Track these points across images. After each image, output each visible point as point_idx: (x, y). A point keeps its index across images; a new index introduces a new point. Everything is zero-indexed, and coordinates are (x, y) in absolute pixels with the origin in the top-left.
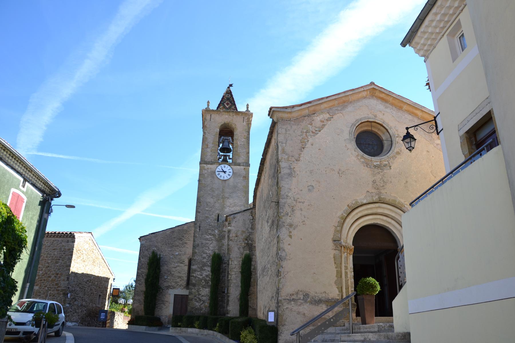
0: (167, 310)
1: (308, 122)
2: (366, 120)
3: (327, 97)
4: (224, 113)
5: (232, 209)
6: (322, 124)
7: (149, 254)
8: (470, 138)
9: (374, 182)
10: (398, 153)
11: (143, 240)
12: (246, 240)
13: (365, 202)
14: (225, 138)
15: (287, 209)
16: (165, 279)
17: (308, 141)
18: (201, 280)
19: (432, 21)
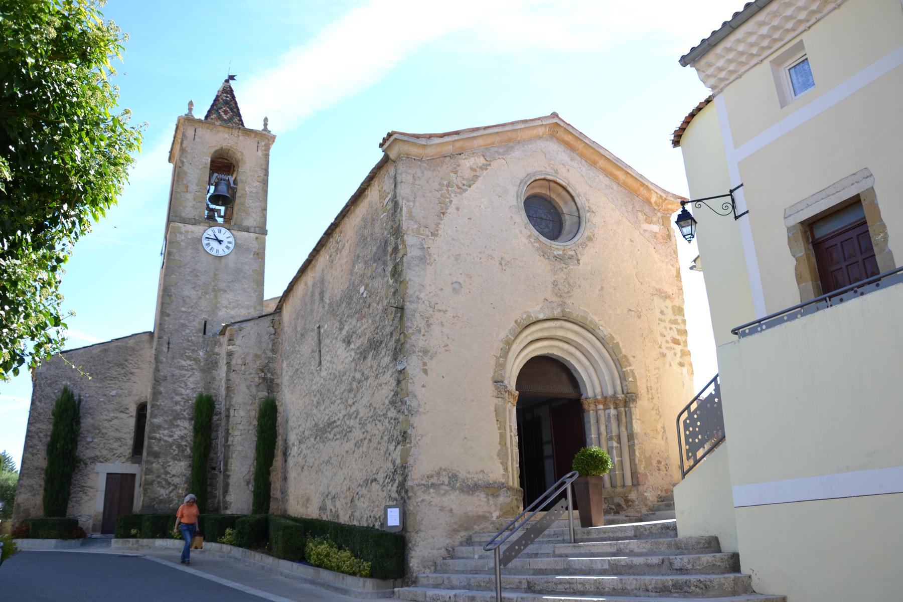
0: (91, 504)
1: (450, 168)
2: (542, 177)
3: (485, 128)
4: (222, 129)
5: (233, 313)
6: (473, 173)
7: (54, 394)
8: (806, 232)
9: (555, 284)
10: (590, 239)
12: (263, 371)
13: (541, 316)
14: (220, 176)
16: (88, 443)
17: (451, 202)
18: (171, 446)
19: (750, 34)
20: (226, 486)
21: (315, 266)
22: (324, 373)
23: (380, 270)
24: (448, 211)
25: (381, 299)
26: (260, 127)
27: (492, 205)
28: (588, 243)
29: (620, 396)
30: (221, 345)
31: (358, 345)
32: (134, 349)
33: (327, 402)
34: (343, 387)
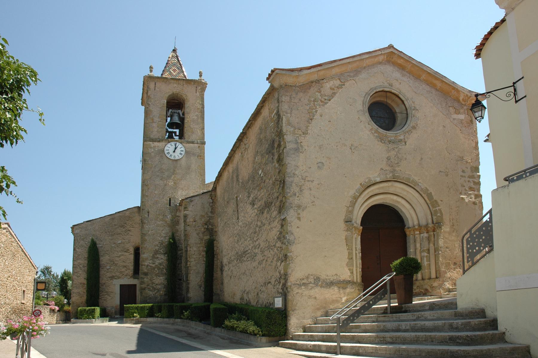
1: (316, 89)
2: (381, 89)
7: (87, 244)
9: (388, 159)
10: (414, 128)
11: (76, 229)
12: (206, 224)
13: (378, 180)
14: (173, 111)
15: (295, 189)
20: (188, 289)
21: (233, 160)
22: (240, 224)
23: (270, 159)
24: (314, 118)
25: (271, 177)
26: (197, 78)
27: (346, 112)
28: (413, 131)
29: (431, 225)
30: (180, 211)
31: (258, 206)
32: (129, 217)
33: (243, 240)
34: (251, 231)
